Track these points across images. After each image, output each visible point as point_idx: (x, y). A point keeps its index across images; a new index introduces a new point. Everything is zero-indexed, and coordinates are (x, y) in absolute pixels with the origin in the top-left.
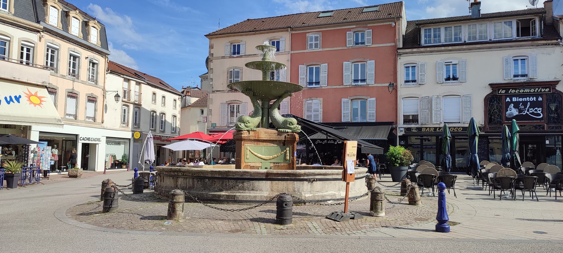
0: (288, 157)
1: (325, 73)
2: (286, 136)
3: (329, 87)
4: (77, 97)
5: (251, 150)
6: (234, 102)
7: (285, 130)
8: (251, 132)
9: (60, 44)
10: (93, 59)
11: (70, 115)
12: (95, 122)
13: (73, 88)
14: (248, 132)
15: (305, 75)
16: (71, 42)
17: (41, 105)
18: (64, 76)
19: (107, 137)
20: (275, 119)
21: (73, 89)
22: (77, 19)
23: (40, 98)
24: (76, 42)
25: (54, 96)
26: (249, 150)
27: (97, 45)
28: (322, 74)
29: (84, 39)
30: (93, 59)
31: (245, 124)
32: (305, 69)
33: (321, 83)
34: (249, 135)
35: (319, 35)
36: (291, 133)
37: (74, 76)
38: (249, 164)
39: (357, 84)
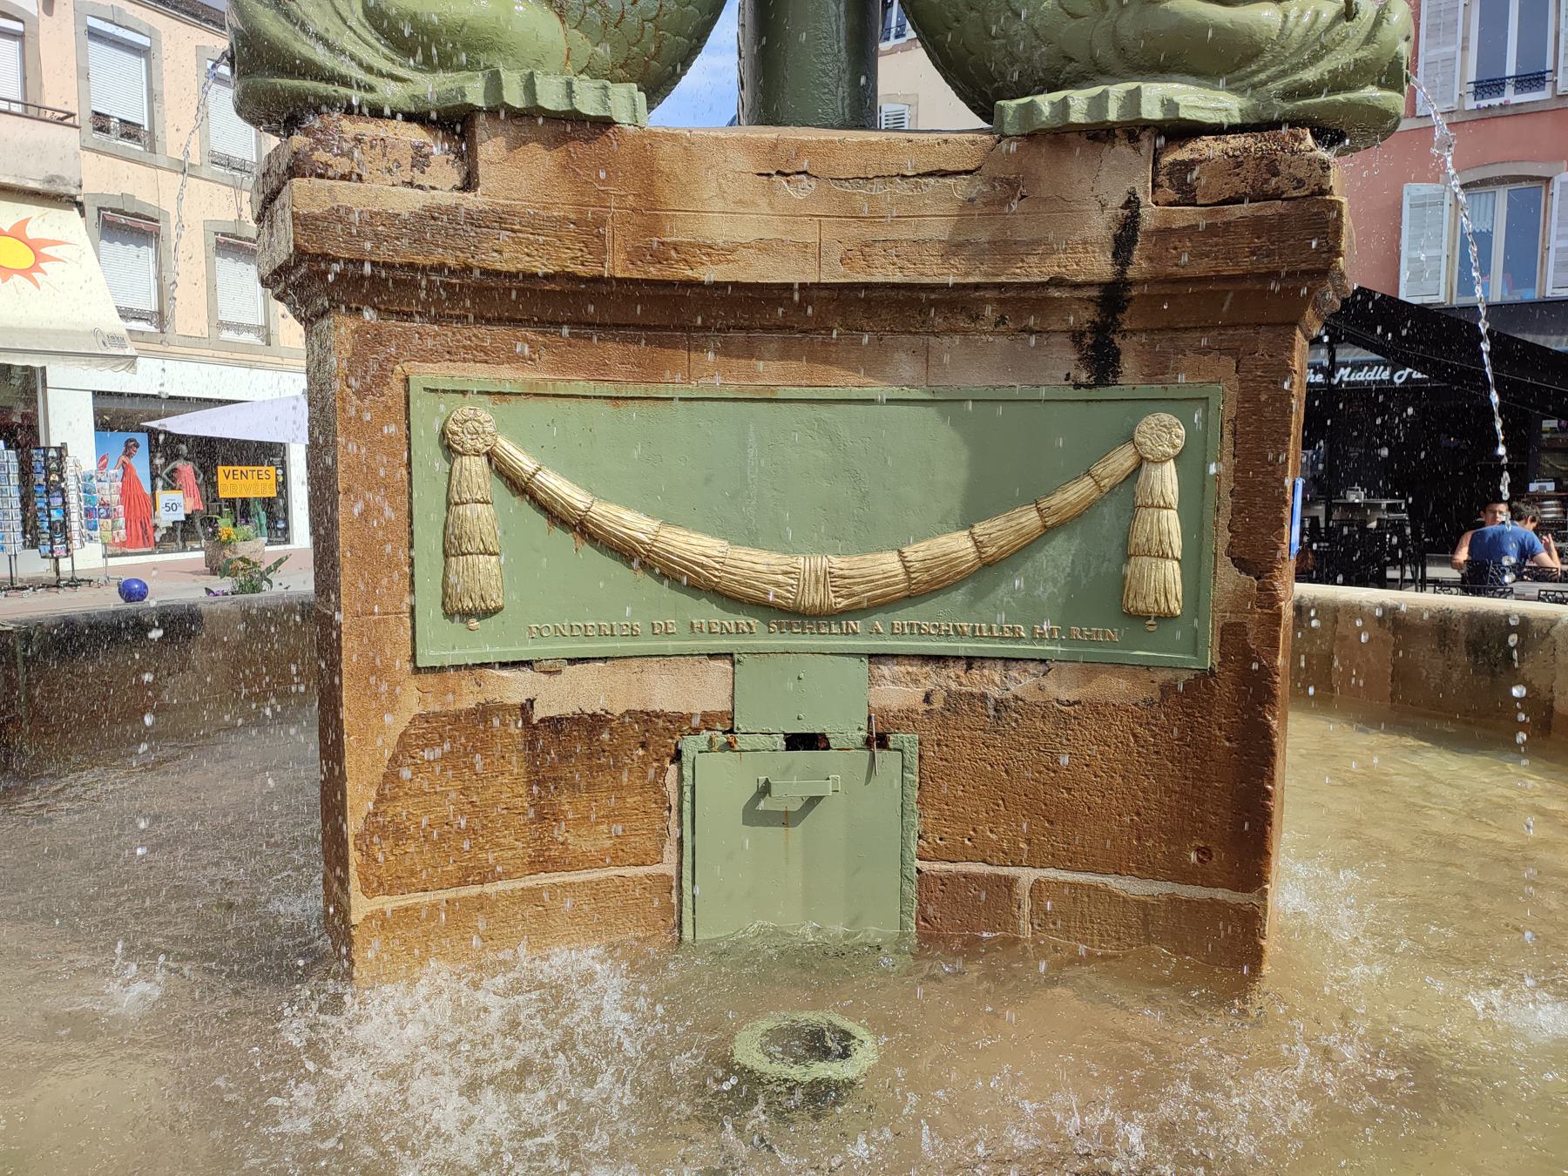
0: (1172, 570)
2: (1132, 203)
4: (158, 235)
5: (524, 462)
8: (491, 148)
9: (151, 28)
11: (239, 327)
12: (162, 332)
13: (240, 216)
14: (438, 149)
16: (204, 21)
17: (35, 275)
19: (94, 392)
23: (35, 246)
25: (151, 251)
34: (471, 200)
36: (1235, 142)
37: (108, 131)
38: (514, 688)
39: (1496, 101)
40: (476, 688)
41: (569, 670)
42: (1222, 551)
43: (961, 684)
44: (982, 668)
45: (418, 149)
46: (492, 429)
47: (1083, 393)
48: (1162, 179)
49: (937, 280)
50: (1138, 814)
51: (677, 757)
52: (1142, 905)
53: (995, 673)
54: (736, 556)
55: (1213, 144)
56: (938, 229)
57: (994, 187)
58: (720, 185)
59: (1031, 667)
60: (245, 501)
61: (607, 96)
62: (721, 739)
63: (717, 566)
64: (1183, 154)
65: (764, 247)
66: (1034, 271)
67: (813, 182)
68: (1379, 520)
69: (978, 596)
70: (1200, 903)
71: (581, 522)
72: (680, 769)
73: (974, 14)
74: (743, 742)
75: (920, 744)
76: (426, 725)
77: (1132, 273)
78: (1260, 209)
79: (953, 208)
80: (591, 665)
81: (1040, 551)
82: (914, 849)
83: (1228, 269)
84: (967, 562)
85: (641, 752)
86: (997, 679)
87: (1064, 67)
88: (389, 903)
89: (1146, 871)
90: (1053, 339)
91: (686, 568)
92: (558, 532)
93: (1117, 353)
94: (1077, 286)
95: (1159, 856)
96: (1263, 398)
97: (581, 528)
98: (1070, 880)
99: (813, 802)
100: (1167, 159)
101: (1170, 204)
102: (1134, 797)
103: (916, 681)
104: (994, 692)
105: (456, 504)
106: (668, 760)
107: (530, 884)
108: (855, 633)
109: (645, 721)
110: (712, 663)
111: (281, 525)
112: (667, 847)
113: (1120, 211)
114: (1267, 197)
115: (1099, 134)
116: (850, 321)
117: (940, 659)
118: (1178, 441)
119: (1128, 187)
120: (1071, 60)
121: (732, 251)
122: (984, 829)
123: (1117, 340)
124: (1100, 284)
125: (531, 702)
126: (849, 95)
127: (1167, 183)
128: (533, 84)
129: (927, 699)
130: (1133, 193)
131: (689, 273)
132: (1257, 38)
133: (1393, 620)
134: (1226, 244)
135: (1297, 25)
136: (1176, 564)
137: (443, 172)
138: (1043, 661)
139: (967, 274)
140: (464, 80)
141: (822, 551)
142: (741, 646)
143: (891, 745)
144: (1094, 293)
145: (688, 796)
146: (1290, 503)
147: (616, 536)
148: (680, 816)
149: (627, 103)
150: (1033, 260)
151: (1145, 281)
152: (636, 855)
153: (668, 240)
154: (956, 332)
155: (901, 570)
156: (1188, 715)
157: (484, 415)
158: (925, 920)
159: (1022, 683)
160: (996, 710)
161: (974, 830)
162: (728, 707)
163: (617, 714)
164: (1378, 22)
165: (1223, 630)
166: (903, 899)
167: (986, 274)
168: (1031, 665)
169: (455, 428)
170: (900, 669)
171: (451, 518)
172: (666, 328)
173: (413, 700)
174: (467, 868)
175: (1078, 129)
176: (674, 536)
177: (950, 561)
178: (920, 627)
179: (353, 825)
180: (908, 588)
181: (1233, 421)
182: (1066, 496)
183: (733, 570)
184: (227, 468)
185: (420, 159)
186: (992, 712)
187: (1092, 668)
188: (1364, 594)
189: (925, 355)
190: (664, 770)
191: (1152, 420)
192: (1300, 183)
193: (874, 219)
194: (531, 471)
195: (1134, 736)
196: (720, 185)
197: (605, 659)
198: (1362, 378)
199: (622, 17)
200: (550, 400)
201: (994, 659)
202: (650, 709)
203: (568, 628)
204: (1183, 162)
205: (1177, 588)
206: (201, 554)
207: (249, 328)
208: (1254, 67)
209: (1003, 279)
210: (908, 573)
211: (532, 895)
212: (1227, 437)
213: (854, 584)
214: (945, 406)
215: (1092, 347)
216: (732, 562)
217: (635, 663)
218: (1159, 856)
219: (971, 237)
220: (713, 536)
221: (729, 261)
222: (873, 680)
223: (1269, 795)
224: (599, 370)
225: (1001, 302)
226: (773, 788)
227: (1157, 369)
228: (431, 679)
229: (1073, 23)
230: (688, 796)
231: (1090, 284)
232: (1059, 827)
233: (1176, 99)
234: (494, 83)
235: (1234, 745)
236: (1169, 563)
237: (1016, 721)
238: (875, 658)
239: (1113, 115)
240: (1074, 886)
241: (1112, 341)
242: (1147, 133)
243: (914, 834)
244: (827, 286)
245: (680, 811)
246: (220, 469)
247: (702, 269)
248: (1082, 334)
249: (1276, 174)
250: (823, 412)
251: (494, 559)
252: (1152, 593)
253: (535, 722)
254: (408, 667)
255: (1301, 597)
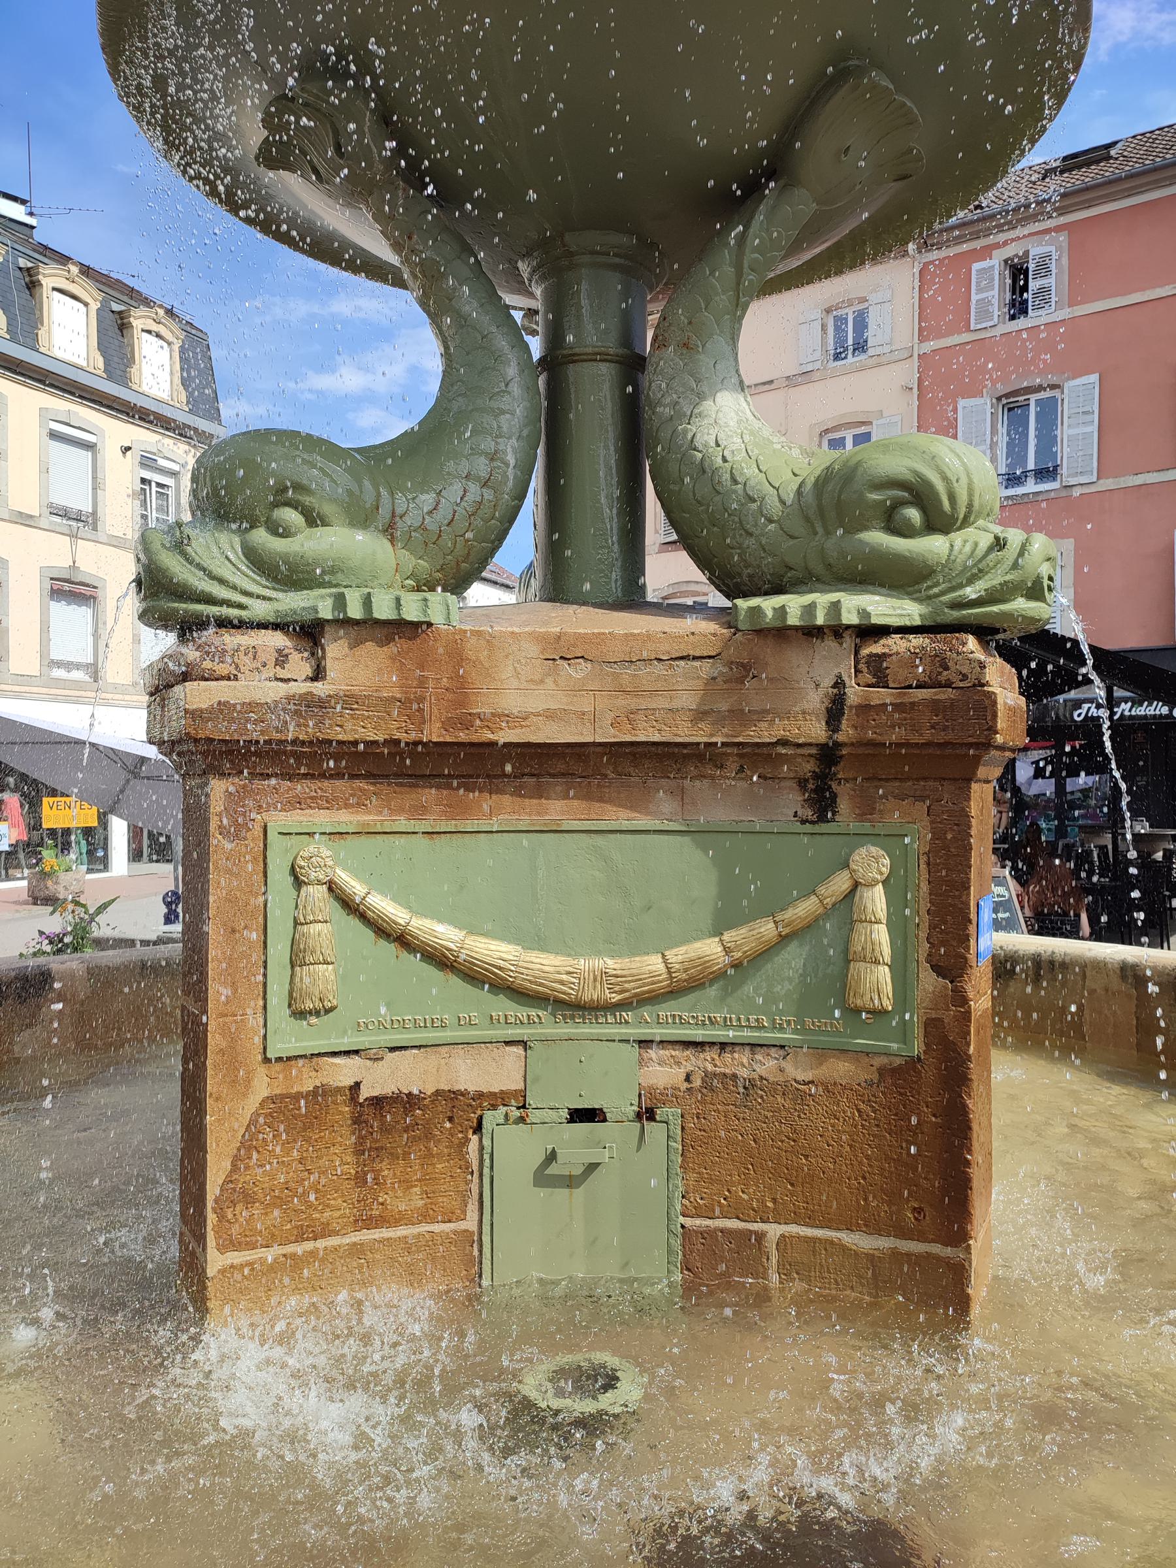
0: (884, 974)
1: (1088, 418)
2: (839, 684)
3: (1108, 484)
4: (95, 598)
5: (356, 887)
6: (684, 588)
7: (822, 600)
8: (335, 649)
10: (154, 454)
11: (69, 666)
15: (988, 442)
18: (31, 517)
20: (702, 469)
21: (74, 567)
22: (74, 297)
24: (73, 386)
26: (332, 887)
27: (171, 403)
28: (1069, 426)
29: (13, 339)
30: (154, 454)
31: (260, 536)
32: (989, 415)
33: (1064, 471)
35: (1053, 249)
36: (917, 641)
38: (344, 1073)
40: (313, 1074)
41: (390, 1056)
42: (922, 959)
43: (715, 1066)
44: (732, 1052)
45: (279, 651)
46: (331, 863)
47: (808, 828)
48: (862, 666)
49: (687, 740)
50: (864, 1178)
51: (478, 1129)
52: (870, 1258)
53: (744, 1057)
54: (528, 959)
55: (900, 642)
56: (688, 700)
57: (731, 669)
58: (515, 668)
59: (773, 1051)
60: (67, 832)
61: (427, 606)
62: (517, 1113)
63: (512, 968)
64: (876, 648)
65: (550, 715)
66: (763, 733)
67: (589, 665)
68: (1165, 850)
69: (725, 995)
70: (919, 1256)
71: (402, 935)
72: (481, 1140)
73: (715, 529)
74: (534, 1116)
75: (682, 1116)
76: (272, 1106)
77: (840, 737)
78: (936, 694)
79: (699, 684)
80: (408, 1052)
81: (777, 955)
82: (678, 1207)
83: (916, 739)
84: (718, 964)
85: (448, 1125)
86: (745, 1061)
87: (786, 573)
88: (235, 1257)
89: (873, 1227)
90: (782, 784)
91: (486, 970)
92: (382, 943)
93: (834, 797)
94: (799, 745)
95: (882, 1214)
96: (949, 836)
97: (403, 940)
98: (809, 1235)
99: (592, 1167)
100: (865, 651)
101: (869, 686)
102: (861, 1163)
103: (678, 1063)
104: (744, 1073)
105: (302, 924)
106: (471, 1131)
107: (354, 1239)
108: (627, 1022)
109: (452, 1099)
110: (507, 1048)
111: (100, 854)
112: (470, 1207)
113: (830, 690)
114: (940, 685)
115: (812, 632)
116: (620, 769)
117: (698, 1045)
118: (884, 869)
119: (836, 671)
120: (791, 569)
121: (525, 719)
122: (737, 1189)
123: (834, 785)
124: (817, 745)
125: (357, 1085)
126: (622, 577)
127: (865, 670)
128: (371, 602)
129: (688, 1078)
130: (840, 677)
131: (491, 736)
132: (930, 563)
133: (1132, 974)
134: (911, 719)
135: (960, 553)
136: (887, 969)
137: (299, 665)
138: (782, 1047)
139: (712, 735)
140: (316, 598)
141: (599, 953)
142: (532, 1035)
143: (658, 1118)
144: (814, 751)
145: (487, 1162)
146: (974, 922)
147: (429, 945)
148: (481, 1175)
149: (442, 608)
150: (763, 725)
151: (852, 744)
152: (444, 1214)
153: (474, 711)
154: (704, 777)
155: (664, 970)
156: (901, 1094)
157: (325, 852)
158: (688, 1269)
159: (766, 1065)
160: (745, 1088)
161: (729, 1191)
162: (521, 1086)
163: (429, 1093)
164: (1021, 554)
165: (926, 1025)
166: (670, 1251)
167: (727, 736)
168: (773, 1050)
169: (302, 863)
170: (665, 1053)
171: (297, 936)
172: (471, 776)
173: (262, 1086)
174: (302, 1226)
175: (796, 628)
176: (478, 944)
177: (703, 963)
178: (680, 1017)
179: (213, 1190)
180: (669, 986)
181: (927, 854)
182: (796, 911)
183: (525, 971)
184: (51, 800)
185: (281, 659)
186: (741, 1090)
187: (821, 1053)
188: (1108, 951)
189: (680, 794)
190: (468, 1140)
191: (863, 851)
192: (965, 677)
193: (636, 693)
194: (363, 895)
195: (859, 1111)
196: (515, 668)
197: (419, 1047)
198: (1143, 713)
199: (440, 536)
200: (378, 836)
201: (743, 1044)
202: (456, 1088)
203: (389, 1021)
204: (877, 655)
205: (888, 989)
206: (25, 883)
207: (78, 666)
208: (929, 583)
209: (740, 739)
210: (670, 973)
211: (357, 1250)
212: (923, 866)
213: (626, 982)
214: (697, 836)
215: (815, 791)
216: (525, 965)
217: (444, 1050)
218: (882, 1214)
219: (714, 707)
220: (509, 942)
221: (522, 727)
222: (642, 1062)
223: (968, 1163)
224: (419, 811)
225: (740, 756)
226: (559, 1156)
227: (867, 809)
228: (278, 1067)
229: (792, 542)
230: (487, 1162)
231: (810, 745)
232: (799, 1189)
233: (869, 609)
234: (340, 602)
235: (939, 1120)
236: (881, 968)
237: (762, 1097)
238: (644, 1043)
239: (820, 621)
240: (814, 1240)
241: (830, 787)
242: (849, 632)
243: (678, 1195)
244: (600, 744)
245: (481, 1175)
246: (45, 800)
247: (501, 733)
248: (806, 780)
249: (947, 668)
250: (599, 840)
251: (330, 967)
252: (868, 992)
253: (361, 1101)
254: (260, 1058)
255: (1053, 953)
